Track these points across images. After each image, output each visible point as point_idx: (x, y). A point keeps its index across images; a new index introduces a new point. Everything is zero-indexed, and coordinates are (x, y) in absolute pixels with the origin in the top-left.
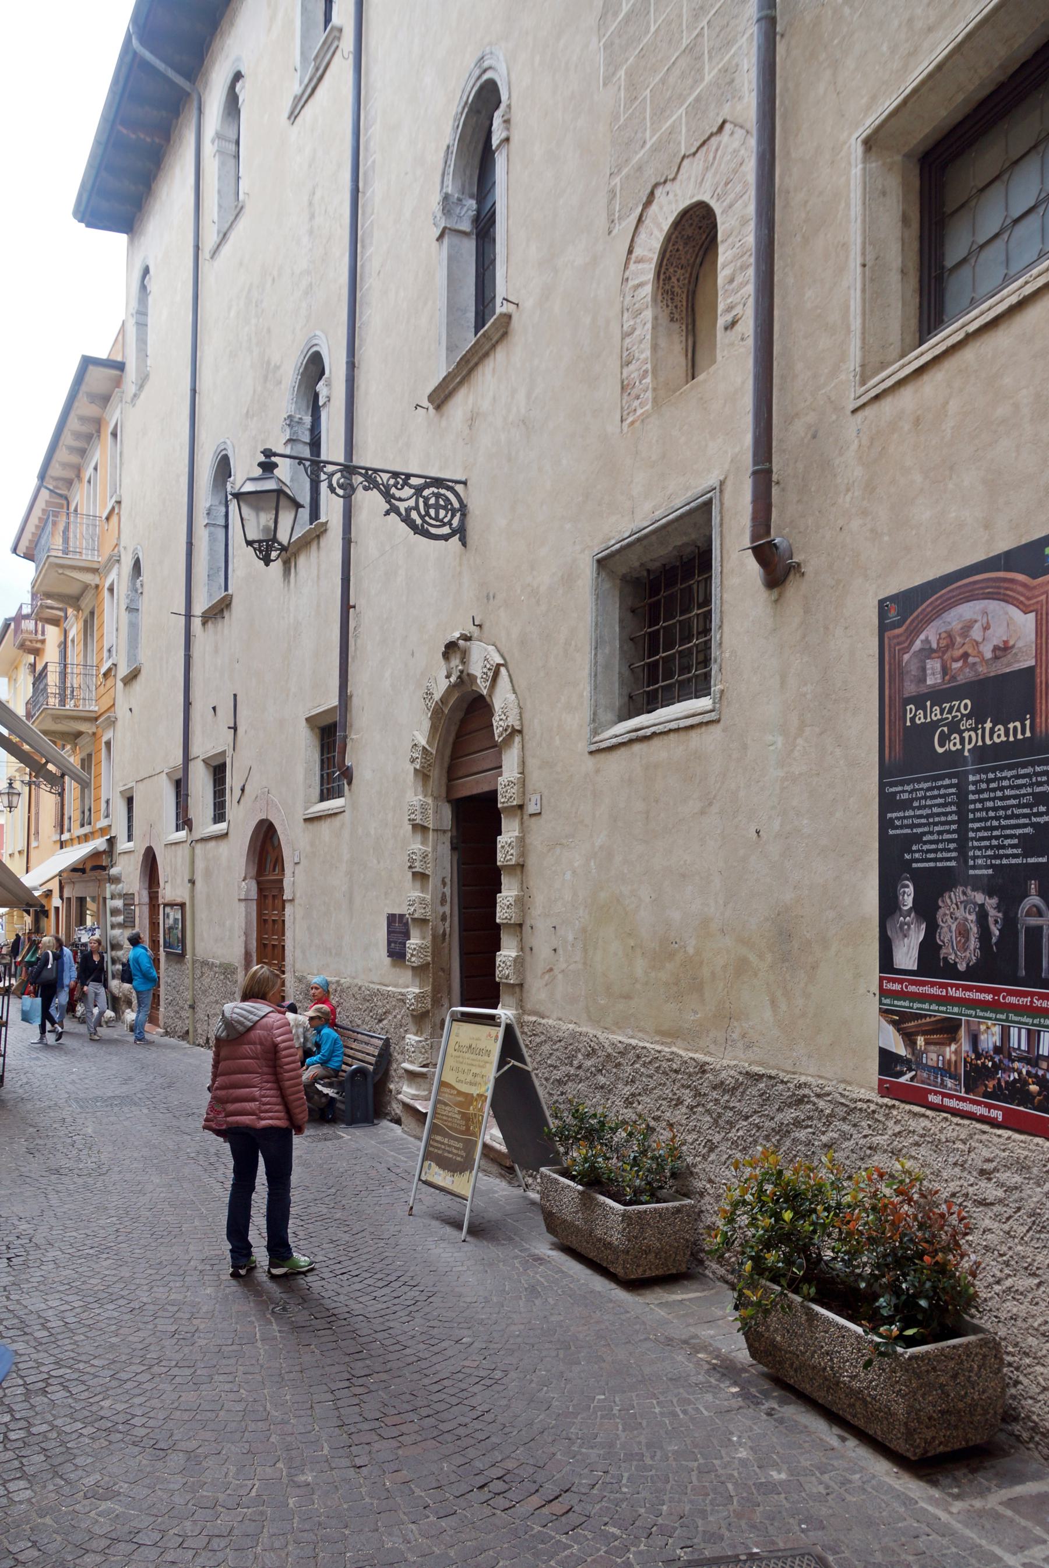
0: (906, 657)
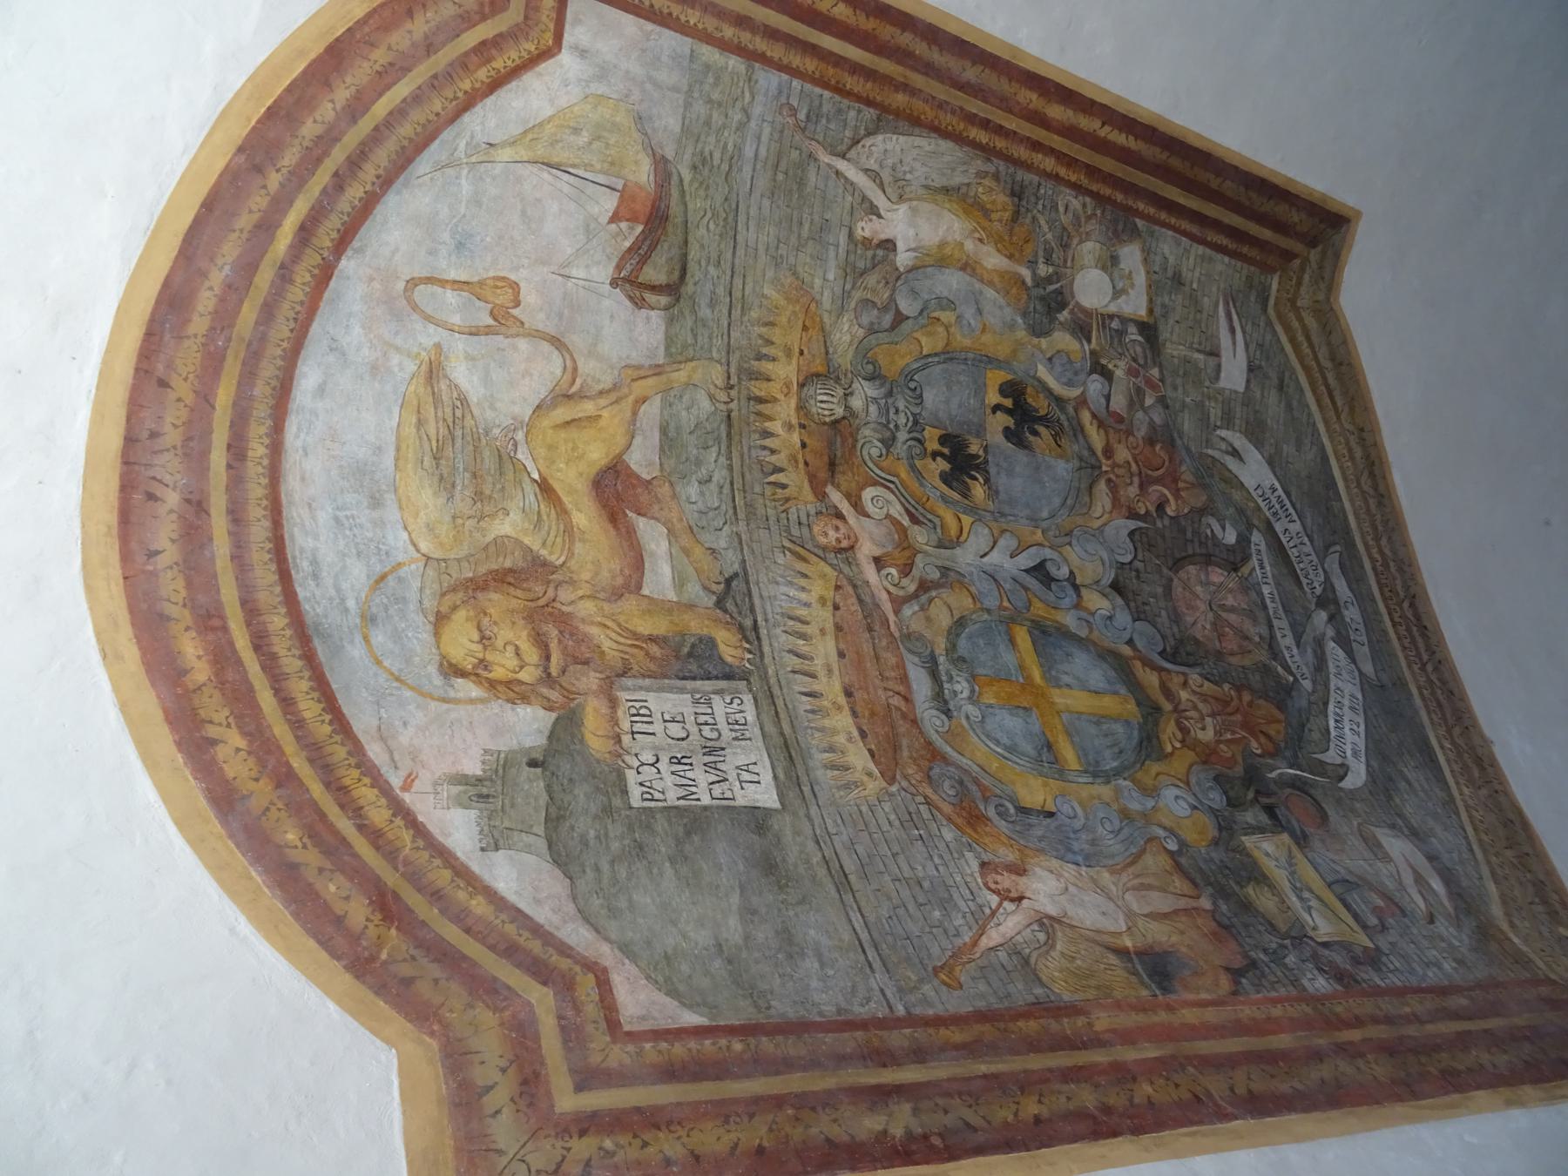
0: (637, 1000)
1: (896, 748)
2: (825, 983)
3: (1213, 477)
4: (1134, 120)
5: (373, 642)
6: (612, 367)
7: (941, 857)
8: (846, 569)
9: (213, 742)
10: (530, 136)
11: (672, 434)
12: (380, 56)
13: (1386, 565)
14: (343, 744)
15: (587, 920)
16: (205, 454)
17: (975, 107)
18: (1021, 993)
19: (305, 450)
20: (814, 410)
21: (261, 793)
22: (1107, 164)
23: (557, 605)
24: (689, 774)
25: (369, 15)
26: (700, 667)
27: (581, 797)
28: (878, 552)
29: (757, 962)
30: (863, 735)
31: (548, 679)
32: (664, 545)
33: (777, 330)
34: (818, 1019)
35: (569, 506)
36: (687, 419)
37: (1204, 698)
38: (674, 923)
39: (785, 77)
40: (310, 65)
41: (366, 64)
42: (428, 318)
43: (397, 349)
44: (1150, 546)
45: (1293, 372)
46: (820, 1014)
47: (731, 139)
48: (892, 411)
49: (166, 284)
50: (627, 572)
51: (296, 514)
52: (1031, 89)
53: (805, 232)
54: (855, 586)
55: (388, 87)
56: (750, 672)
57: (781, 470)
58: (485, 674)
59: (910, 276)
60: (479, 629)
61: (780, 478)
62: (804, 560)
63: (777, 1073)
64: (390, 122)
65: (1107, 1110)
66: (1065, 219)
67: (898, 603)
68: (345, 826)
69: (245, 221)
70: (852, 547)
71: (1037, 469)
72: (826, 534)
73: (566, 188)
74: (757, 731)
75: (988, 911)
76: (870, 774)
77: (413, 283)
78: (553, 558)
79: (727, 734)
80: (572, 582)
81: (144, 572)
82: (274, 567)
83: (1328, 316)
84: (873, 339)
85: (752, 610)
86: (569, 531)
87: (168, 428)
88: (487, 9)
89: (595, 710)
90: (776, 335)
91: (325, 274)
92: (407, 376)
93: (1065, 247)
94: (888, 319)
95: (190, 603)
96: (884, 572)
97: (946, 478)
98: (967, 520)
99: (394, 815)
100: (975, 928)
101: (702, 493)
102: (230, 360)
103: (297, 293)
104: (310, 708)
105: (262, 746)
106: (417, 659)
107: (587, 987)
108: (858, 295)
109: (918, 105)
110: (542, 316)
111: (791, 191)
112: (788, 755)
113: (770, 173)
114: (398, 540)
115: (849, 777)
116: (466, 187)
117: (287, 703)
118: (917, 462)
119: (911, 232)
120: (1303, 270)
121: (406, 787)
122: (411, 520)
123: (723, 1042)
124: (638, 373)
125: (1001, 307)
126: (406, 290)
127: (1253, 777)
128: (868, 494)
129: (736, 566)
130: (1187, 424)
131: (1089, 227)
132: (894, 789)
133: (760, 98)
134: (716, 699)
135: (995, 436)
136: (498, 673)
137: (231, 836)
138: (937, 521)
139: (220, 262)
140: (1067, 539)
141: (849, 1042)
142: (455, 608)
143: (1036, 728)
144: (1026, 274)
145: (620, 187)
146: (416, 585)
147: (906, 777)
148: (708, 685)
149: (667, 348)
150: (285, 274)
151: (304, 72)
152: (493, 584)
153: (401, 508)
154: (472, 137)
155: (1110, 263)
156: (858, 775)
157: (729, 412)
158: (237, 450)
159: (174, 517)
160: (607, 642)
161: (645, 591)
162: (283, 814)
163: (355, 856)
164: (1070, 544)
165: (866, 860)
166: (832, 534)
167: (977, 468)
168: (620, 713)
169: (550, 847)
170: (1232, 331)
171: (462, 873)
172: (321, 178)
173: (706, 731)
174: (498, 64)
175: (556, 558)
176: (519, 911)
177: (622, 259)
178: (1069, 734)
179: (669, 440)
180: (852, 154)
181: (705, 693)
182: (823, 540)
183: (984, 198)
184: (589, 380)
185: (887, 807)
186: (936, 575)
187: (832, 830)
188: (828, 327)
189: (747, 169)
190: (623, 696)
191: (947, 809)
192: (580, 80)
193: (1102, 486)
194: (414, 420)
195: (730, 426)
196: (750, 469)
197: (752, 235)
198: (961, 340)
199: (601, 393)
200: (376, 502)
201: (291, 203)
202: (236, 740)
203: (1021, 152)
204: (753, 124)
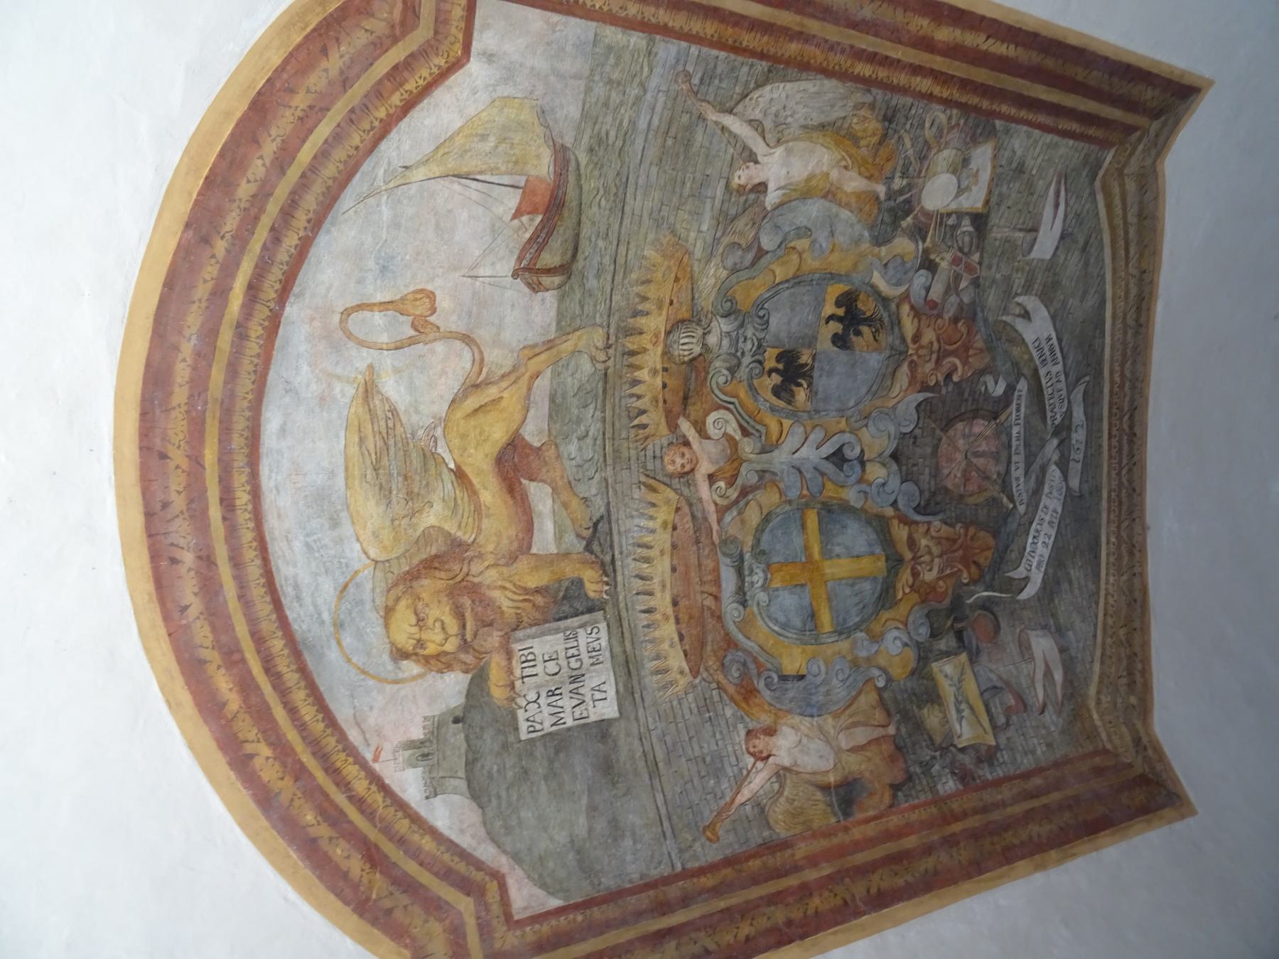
0: (525, 896)
1: (703, 644)
2: (635, 860)
3: (1005, 336)
4: (1020, 29)
5: (344, 643)
6: (512, 351)
7: (721, 732)
8: (686, 491)
9: (251, 757)
10: (441, 152)
12: (300, 101)
13: (1122, 386)
14: (333, 735)
16: (205, 511)
17: (866, 42)
18: (757, 836)
19: (277, 488)
20: (676, 353)
21: (286, 788)
22: (982, 75)
23: (470, 578)
24: (560, 703)
25: (286, 62)
27: (489, 741)
28: (712, 469)
29: (595, 848)
30: (681, 637)
31: (465, 646)
32: (549, 502)
33: (652, 287)
34: (628, 886)
35: (478, 486)
36: (571, 383)
37: (938, 541)
38: (545, 829)
39: (684, 44)
40: (237, 125)
41: (288, 113)
42: (362, 344)
43: (339, 378)
45: (1100, 231)
46: (630, 881)
47: (626, 114)
48: (741, 340)
49: (148, 365)
50: (521, 535)
51: (277, 548)
52: (924, 15)
53: (686, 191)
54: (690, 505)
55: (311, 131)
56: (606, 602)
57: (643, 412)
58: (421, 652)
59: (776, 212)
60: (416, 614)
61: (644, 419)
62: (654, 490)
63: (602, 933)
64: (313, 168)
65: (789, 923)
66: (928, 133)
67: (722, 511)
68: (340, 799)
69: (202, 291)
70: (693, 470)
71: (853, 366)
72: (673, 462)
73: (475, 195)
74: (608, 654)
75: (745, 772)
76: (682, 672)
77: (347, 313)
78: (466, 537)
79: (587, 662)
80: (480, 556)
81: (180, 626)
82: (268, 599)
83: (1149, 181)
84: (734, 278)
85: (612, 547)
86: (478, 510)
87: (174, 496)
88: (397, 32)
89: (498, 664)
90: (651, 291)
91: (275, 321)
92: (348, 400)
93: (922, 158)
94: (750, 256)
95: (217, 645)
96: (715, 487)
97: (777, 391)
99: (370, 783)
100: (735, 787)
101: (580, 449)
102: (209, 421)
103: (253, 347)
104: (308, 712)
105: (283, 751)
106: (374, 651)
107: (493, 887)
108: (726, 240)
109: (811, 50)
110: (454, 318)
111: (677, 154)
113: (660, 141)
114: (353, 551)
115: (668, 678)
116: (386, 213)
117: (292, 711)
118: (755, 382)
119: (784, 172)
120: (1140, 140)
121: (376, 760)
122: (361, 532)
123: (571, 916)
124: (532, 351)
125: (852, 226)
126: (341, 321)
127: (956, 608)
129: (603, 509)
130: (992, 299)
131: (950, 136)
132: (697, 681)
133: (658, 70)
134: (581, 631)
135: (824, 343)
136: (431, 649)
137: (274, 827)
138: (763, 430)
139: (187, 333)
141: (644, 900)
142: (398, 599)
143: (806, 602)
144: (881, 190)
145: (522, 184)
146: (370, 588)
147: (707, 669)
149: (558, 323)
150: (241, 333)
151: (233, 134)
152: (423, 572)
153: (353, 523)
154: (389, 164)
155: (961, 166)
156: (674, 675)
157: (607, 369)
158: (228, 503)
159: (192, 573)
160: (505, 602)
161: (534, 550)
162: (303, 801)
163: (350, 822)
164: (866, 426)
166: (679, 461)
167: (804, 376)
168: (514, 662)
169: (469, 786)
170: (1057, 205)
171: (415, 819)
172: (261, 235)
174: (410, 86)
175: (468, 538)
176: (451, 842)
177: (522, 250)
178: (829, 600)
179: (556, 405)
180: (740, 108)
181: (574, 629)
182: (670, 468)
183: (857, 127)
184: (493, 368)
185: (690, 697)
186: (754, 479)
187: (652, 727)
188: (696, 275)
189: (640, 141)
190: (516, 647)
191: (731, 689)
192: (487, 86)
193: (905, 368)
194: (357, 440)
195: (606, 382)
197: (638, 203)
198: (812, 263)
199: (503, 376)
200: (335, 523)
201: (238, 265)
202: (265, 751)
203: (901, 79)
204: (649, 96)
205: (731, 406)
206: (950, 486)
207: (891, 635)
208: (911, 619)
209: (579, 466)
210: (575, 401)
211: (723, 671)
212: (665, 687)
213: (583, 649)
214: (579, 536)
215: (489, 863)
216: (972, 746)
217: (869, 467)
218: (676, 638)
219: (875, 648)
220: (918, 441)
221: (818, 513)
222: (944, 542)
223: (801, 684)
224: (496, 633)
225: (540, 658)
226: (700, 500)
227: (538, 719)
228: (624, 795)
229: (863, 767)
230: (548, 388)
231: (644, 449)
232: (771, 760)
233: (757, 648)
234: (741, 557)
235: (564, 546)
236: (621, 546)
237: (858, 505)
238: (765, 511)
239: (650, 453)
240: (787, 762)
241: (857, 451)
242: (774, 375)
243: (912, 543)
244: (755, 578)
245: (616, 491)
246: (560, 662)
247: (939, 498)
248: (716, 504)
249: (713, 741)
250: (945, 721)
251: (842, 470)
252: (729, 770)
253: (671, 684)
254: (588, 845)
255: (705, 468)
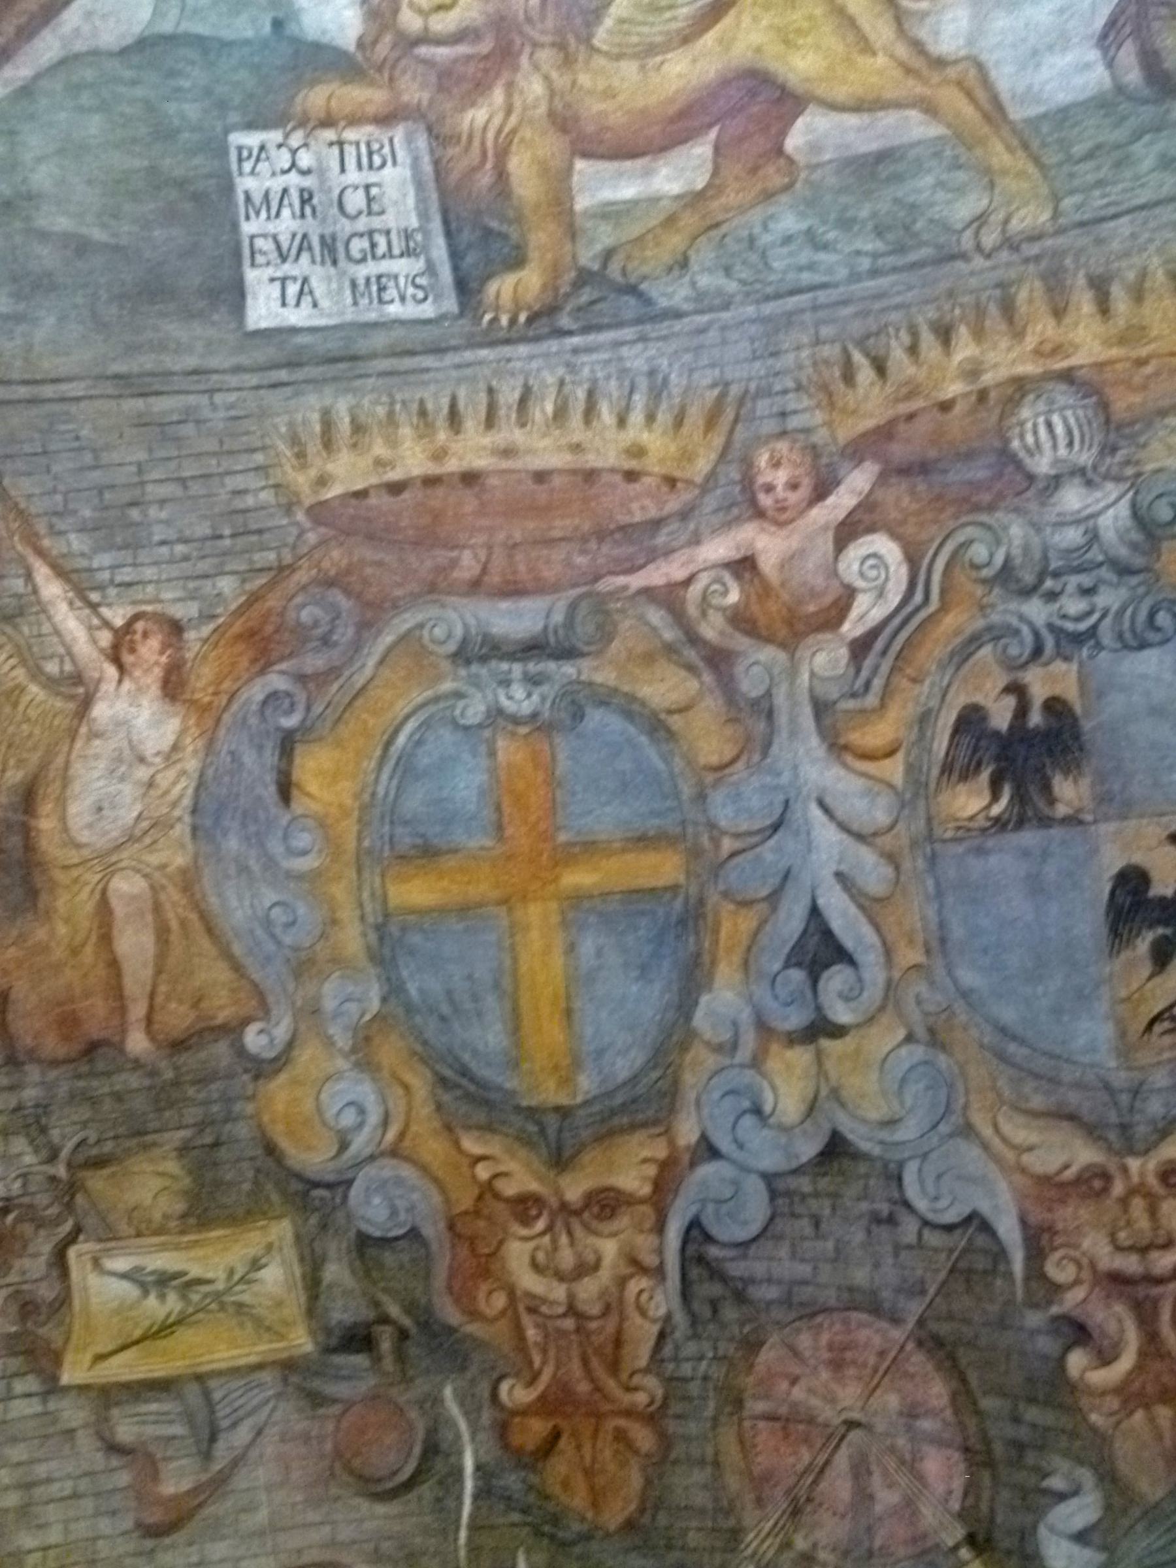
7: (186, 558)
11: (884, 171)
15: (62, 62)
20: (1025, 413)
23: (527, 50)
24: (286, 212)
26: (470, 246)
28: (768, 564)
30: (396, 488)
32: (675, 188)
37: (612, 1306)
44: (962, 1274)
48: (1086, 580)
54: (684, 515)
57: (880, 368)
61: (865, 374)
62: (711, 421)
67: (669, 597)
70: (760, 514)
72: (776, 464)
74: (372, 316)
75: (95, 597)
79: (362, 272)
85: (587, 329)
89: (369, 101)
96: (727, 577)
97: (970, 720)
98: (894, 770)
100: (69, 565)
101: (787, 240)
112: (334, 357)
115: (314, 447)
118: (986, 651)
124: (976, 81)
127: (432, 1342)
128: (883, 545)
129: (663, 303)
132: (300, 516)
134: (419, 264)
138: (871, 700)
140: (921, 1032)
143: (459, 836)
147: (323, 542)
148: (439, 250)
156: (318, 463)
157: (963, 256)
161: (580, 164)
164: (910, 1038)
165: (170, 430)
166: (781, 477)
167: (1020, 797)
173: (358, 246)
175: (601, 36)
178: (464, 910)
179: (874, 168)
181: (426, 248)
182: (763, 460)
185: (266, 496)
186: (750, 684)
187: (218, 398)
190: (399, 133)
193: (1086, 1155)
196: (864, 314)
205: (918, 597)
206: (767, 1356)
207: (366, 1091)
208: (407, 1172)
209: (752, 240)
210: (884, 207)
211: (315, 581)
212: (294, 440)
213: (386, 266)
214: (608, 255)
215: (27, 48)
216: (63, 1301)
217: (801, 1056)
218: (394, 475)
219: (343, 1041)
220: (883, 1232)
221: (674, 889)
222: (611, 1325)
223: (270, 792)
224: (425, 96)
225: (373, 178)
226: (696, 540)
227: (263, 167)
228: (94, 315)
229: (62, 930)
230: (905, 139)
231: (799, 388)
232: (111, 671)
233: (360, 681)
234: (568, 653)
235: (589, 224)
236: (588, 350)
237: (700, 1020)
238: (676, 722)
239: (792, 402)
240: (101, 711)
241: (842, 1014)
242: (1011, 701)
243: (606, 1204)
244: (518, 691)
245: (702, 331)
246: (370, 263)
247: (730, 1313)
248: (688, 581)
249: (171, 534)
250: (145, 1229)
251: (787, 965)
252: (104, 559)
253: (301, 455)
254: (18, 225)
255: (769, 546)
